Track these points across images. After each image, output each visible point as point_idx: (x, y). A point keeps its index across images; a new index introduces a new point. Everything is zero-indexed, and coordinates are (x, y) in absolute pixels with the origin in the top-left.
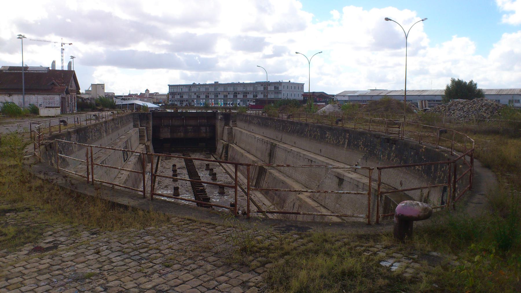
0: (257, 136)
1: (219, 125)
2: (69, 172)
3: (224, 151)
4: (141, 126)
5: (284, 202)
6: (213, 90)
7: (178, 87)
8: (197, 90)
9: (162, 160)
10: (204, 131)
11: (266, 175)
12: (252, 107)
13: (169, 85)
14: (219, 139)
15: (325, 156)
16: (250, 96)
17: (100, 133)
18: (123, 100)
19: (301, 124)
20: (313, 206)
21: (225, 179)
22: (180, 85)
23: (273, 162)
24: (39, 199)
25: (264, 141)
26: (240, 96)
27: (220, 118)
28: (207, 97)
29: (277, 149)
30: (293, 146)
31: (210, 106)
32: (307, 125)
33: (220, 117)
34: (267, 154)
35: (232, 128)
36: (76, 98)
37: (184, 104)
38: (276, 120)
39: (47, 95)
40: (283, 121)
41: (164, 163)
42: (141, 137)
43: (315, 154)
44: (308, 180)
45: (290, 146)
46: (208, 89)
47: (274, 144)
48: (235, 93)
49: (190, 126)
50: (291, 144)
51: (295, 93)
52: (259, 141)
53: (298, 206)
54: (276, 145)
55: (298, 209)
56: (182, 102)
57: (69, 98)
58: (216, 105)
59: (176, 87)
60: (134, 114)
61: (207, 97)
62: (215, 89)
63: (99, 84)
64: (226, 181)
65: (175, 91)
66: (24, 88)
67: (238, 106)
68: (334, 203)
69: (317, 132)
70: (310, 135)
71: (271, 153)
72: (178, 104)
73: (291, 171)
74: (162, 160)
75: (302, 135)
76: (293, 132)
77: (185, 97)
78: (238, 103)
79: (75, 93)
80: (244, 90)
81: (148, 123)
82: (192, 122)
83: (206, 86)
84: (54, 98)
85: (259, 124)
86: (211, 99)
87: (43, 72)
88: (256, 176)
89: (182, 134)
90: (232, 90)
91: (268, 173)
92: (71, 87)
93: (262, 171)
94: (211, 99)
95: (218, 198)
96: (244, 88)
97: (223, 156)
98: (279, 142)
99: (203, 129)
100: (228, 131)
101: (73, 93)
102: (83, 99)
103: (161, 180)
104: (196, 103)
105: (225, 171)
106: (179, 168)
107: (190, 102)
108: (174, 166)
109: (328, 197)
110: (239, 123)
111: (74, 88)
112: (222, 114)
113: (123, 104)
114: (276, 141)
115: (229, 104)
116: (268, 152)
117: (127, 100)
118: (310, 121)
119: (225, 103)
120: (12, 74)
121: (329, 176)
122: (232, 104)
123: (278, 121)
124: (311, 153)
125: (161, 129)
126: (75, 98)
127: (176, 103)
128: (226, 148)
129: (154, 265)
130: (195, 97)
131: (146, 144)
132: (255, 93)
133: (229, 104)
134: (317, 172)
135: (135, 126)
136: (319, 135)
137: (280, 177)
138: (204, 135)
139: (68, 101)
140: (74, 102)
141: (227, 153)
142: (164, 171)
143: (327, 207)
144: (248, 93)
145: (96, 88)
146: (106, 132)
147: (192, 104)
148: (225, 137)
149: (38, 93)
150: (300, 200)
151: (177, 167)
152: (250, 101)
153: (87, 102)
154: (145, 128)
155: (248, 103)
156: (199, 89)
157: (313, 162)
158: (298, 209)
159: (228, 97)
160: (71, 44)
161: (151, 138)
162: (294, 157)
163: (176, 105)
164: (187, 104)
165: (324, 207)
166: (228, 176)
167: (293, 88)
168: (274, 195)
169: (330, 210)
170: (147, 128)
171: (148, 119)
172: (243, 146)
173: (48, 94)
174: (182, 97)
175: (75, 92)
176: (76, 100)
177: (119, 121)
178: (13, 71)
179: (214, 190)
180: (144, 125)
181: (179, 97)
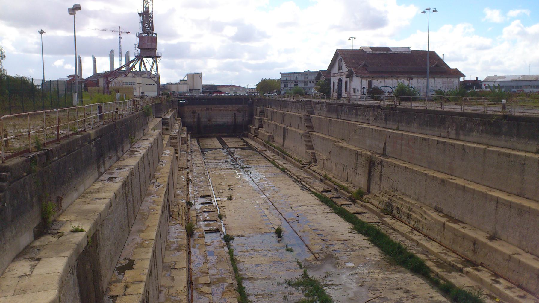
12: (289, 95)
22: (295, 73)
24: (292, 281)
59: (289, 75)
63: (196, 74)
65: (289, 79)
66: (428, 70)
84: (454, 81)
87: (407, 52)
144: (289, 83)
145: (193, 77)
160: (129, 32)
173: (447, 78)
178: (377, 52)
181: (293, 85)
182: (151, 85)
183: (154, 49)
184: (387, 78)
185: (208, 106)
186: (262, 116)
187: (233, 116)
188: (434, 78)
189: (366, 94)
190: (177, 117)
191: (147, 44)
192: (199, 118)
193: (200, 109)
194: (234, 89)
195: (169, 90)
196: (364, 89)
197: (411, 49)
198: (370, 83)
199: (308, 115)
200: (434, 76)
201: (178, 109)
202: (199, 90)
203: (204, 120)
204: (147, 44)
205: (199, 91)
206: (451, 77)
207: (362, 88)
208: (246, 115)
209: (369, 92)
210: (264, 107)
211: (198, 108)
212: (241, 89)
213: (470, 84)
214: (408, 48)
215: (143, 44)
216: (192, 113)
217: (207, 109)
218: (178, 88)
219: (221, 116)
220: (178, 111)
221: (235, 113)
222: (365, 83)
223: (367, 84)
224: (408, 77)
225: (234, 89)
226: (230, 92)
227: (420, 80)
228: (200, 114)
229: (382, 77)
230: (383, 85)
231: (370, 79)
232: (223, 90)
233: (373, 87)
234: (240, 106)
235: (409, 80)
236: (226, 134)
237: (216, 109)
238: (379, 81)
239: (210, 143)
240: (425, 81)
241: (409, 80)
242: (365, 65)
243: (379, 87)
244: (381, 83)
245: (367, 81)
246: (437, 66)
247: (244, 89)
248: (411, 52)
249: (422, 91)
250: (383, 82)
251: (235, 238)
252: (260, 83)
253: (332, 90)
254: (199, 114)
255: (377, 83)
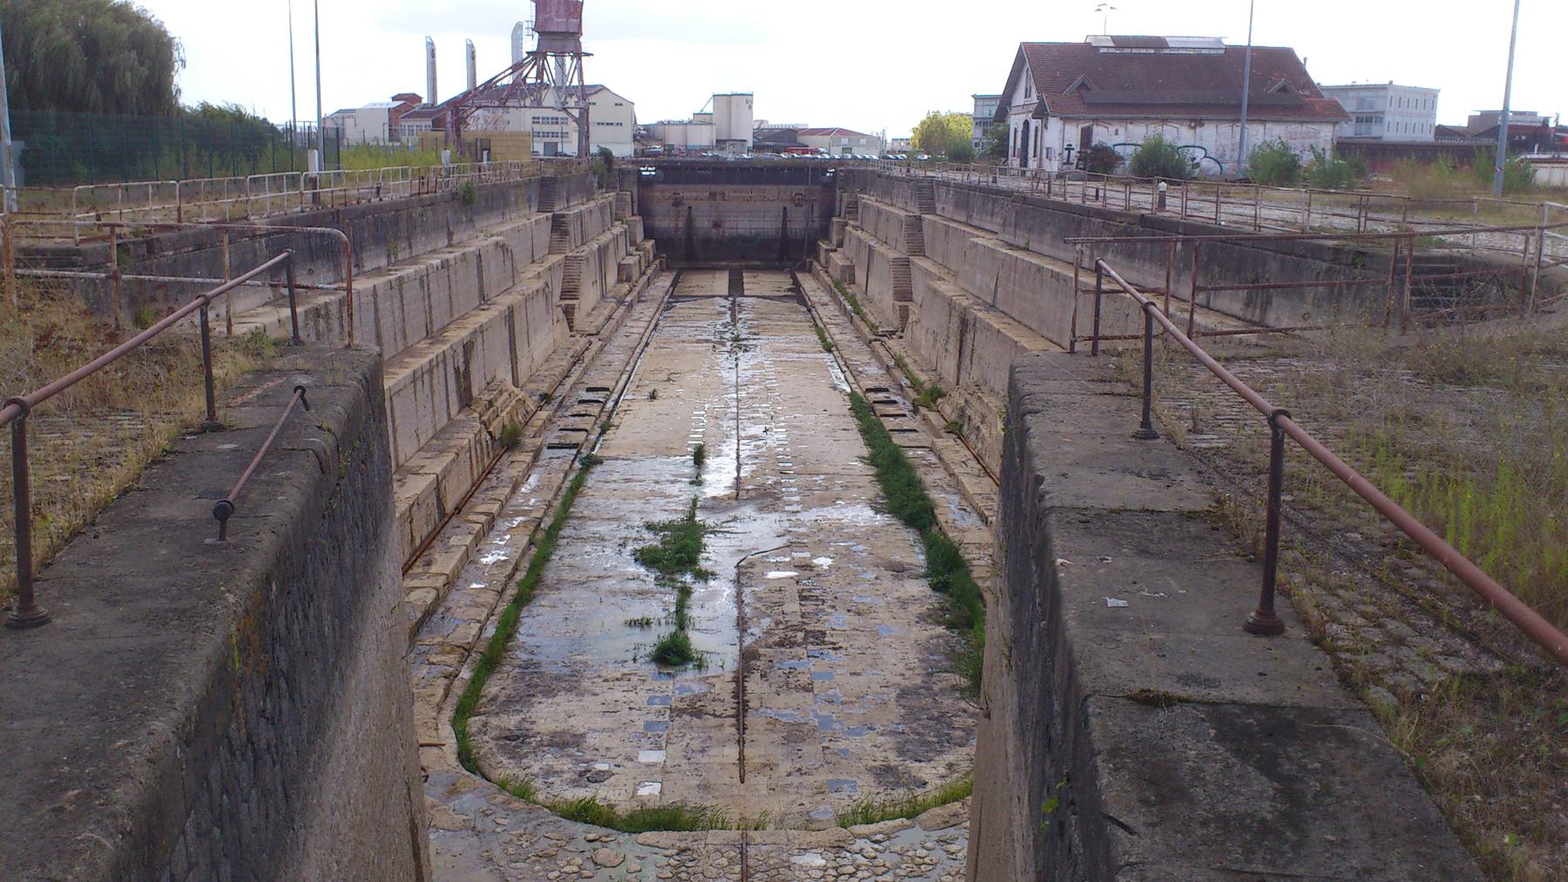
2: (786, 350)
13: (976, 98)
39: (1299, 125)
51: (1415, 120)
63: (737, 95)
83: (1362, 94)
87: (1212, 52)
120: (1132, 57)
129: (931, 867)
145: (729, 103)
149: (1274, 118)
167: (1412, 104)
173: (1301, 123)
182: (610, 127)
183: (573, 34)
184: (1132, 121)
185: (714, 188)
186: (851, 216)
187: (781, 214)
188: (1263, 122)
189: (1075, 162)
190: (633, 215)
191: (556, 20)
192: (690, 220)
193: (694, 194)
194: (845, 141)
195: (661, 141)
196: (1069, 149)
197: (1227, 42)
198: (1086, 135)
199: (918, 214)
200: (1263, 118)
201: (635, 196)
202: (744, 141)
203: (703, 223)
204: (556, 20)
205: (742, 145)
206: (1314, 122)
207: (1065, 146)
208: (816, 215)
209: (1082, 157)
210: (859, 192)
211: (688, 193)
212: (863, 141)
213: (1524, 138)
214: (1219, 41)
215: (546, 20)
216: (673, 205)
217: (713, 195)
218: (685, 133)
219: (748, 214)
220: (636, 199)
221: (785, 209)
222: (1073, 134)
223: (1079, 137)
224: (1191, 120)
225: (845, 141)
226: (833, 149)
227: (1225, 128)
228: (693, 208)
229: (1121, 120)
230: (1121, 139)
231: (1087, 124)
232: (812, 142)
233: (1093, 144)
234: (801, 189)
235: (1194, 128)
236: (758, 263)
237: (736, 194)
238: (1112, 129)
239: (703, 284)
240: (1237, 129)
241: (1194, 128)
242: (1083, 86)
243: (1110, 144)
244: (1116, 133)
245: (1080, 130)
246: (1283, 89)
247: (873, 141)
248: (1223, 52)
249: (1227, 158)
250: (1122, 131)
251: (606, 462)
252: (923, 123)
253: (1011, 152)
254: (690, 208)
255: (1104, 135)
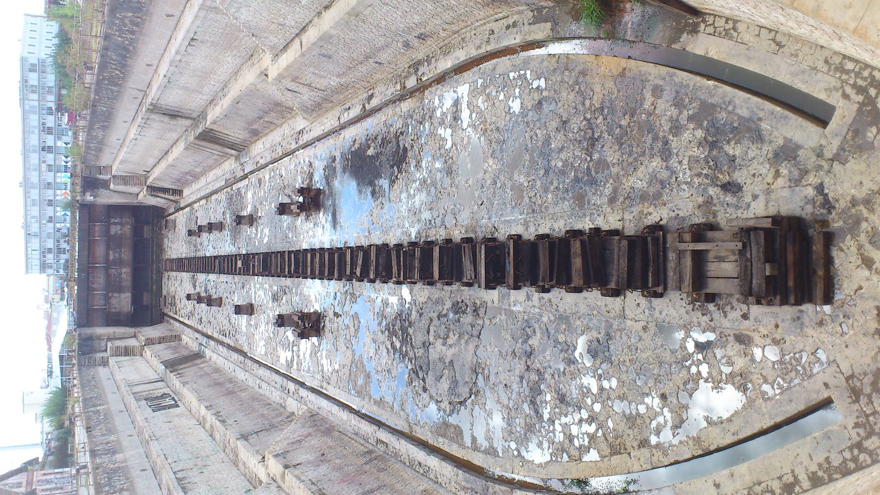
0: (132, 135)
1: (106, 198)
3: (163, 195)
4: (106, 350)
5: (278, 104)
6: (37, 191)
7: (30, 256)
8: (37, 222)
9: (176, 314)
10: (119, 227)
11: (219, 129)
14: (136, 201)
15: (181, 8)
16: (50, 121)
17: (115, 471)
18: (51, 375)
19: (106, 49)
20: (298, 54)
21: (221, 205)
23: (189, 112)
25: (142, 125)
26: (50, 140)
27: (92, 198)
28: (50, 203)
29: (162, 102)
30: (156, 70)
31: (69, 198)
32: (107, 37)
33: (89, 198)
34: (174, 122)
35: (114, 177)
36: (44, 472)
37: (64, 245)
38: (95, 95)
40: (99, 83)
41: (182, 311)
42: (127, 352)
43: (177, 29)
44: (234, 53)
45: (156, 76)
46: (33, 200)
47: (151, 107)
48: (43, 149)
49: (107, 255)
50: (152, 73)
52: (141, 134)
53: (293, 83)
54: (152, 104)
55: (300, 83)
56: (60, 251)
57: (44, 487)
58: (69, 188)
60: (80, 365)
61: (50, 203)
62: (33, 187)
64: (225, 205)
65: (36, 263)
67: (69, 146)
68: (298, 9)
69: (125, 17)
70: (133, 33)
71: (170, 115)
72: (64, 257)
73: (212, 82)
74: (176, 314)
75: (131, 48)
76: (124, 67)
77: (50, 244)
78: (64, 145)
79: (35, 476)
80: (36, 131)
81: (99, 338)
82: (100, 250)
85: (105, 128)
86: (55, 195)
88: (219, 147)
89: (124, 270)
90: (36, 156)
91: (215, 127)
92: (19, 485)
93: (209, 137)
94: (55, 195)
95: (262, 231)
96: (33, 132)
97: (171, 198)
98: (146, 95)
99: (115, 230)
100: (118, 184)
101: (34, 479)
102: (48, 453)
103: (218, 328)
104: (63, 225)
105: (203, 202)
106: (195, 287)
107: (60, 235)
108: (189, 297)
109: (282, 20)
110: (104, 161)
111: (22, 478)
112: (84, 193)
113: (59, 374)
114: (144, 101)
115: (66, 162)
116: (166, 119)
117: (51, 368)
118: (98, 29)
119: (63, 169)
121: (233, 10)
122: (67, 157)
123: (97, 92)
124: (173, 36)
125: (114, 310)
126: (45, 474)
127: (62, 261)
128: (154, 190)
130: (51, 225)
131: (143, 344)
132: (45, 112)
133: (66, 162)
134: (220, 31)
135: (105, 363)
136: (131, 14)
137: (225, 107)
138: (128, 229)
139: (51, 490)
140: (52, 476)
141: (165, 190)
142: (198, 317)
143: (304, 25)
144: (44, 124)
146: (114, 453)
147: (65, 231)
148: (135, 189)
150: (280, 78)
151: (192, 291)
152: (59, 122)
153: (55, 448)
154: (109, 344)
155: (64, 126)
156: (33, 217)
157: (195, 37)
158: (300, 83)
159: (52, 163)
161: (131, 330)
162: (181, 73)
163: (67, 261)
164: (65, 241)
165: (303, 30)
166: (214, 197)
168: (261, 121)
169: (311, 18)
170: (109, 339)
171: (90, 338)
172: (151, 161)
174: (50, 251)
175: (33, 475)
176: (49, 471)
177: (92, 409)
179: (244, 233)
180: (103, 344)
